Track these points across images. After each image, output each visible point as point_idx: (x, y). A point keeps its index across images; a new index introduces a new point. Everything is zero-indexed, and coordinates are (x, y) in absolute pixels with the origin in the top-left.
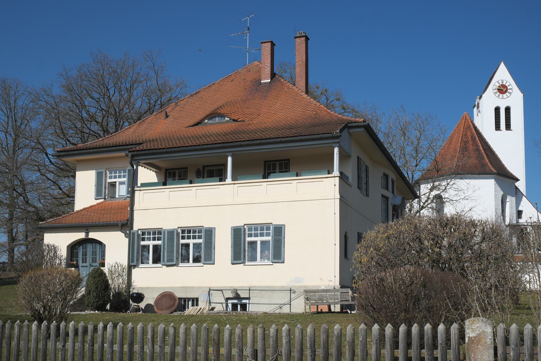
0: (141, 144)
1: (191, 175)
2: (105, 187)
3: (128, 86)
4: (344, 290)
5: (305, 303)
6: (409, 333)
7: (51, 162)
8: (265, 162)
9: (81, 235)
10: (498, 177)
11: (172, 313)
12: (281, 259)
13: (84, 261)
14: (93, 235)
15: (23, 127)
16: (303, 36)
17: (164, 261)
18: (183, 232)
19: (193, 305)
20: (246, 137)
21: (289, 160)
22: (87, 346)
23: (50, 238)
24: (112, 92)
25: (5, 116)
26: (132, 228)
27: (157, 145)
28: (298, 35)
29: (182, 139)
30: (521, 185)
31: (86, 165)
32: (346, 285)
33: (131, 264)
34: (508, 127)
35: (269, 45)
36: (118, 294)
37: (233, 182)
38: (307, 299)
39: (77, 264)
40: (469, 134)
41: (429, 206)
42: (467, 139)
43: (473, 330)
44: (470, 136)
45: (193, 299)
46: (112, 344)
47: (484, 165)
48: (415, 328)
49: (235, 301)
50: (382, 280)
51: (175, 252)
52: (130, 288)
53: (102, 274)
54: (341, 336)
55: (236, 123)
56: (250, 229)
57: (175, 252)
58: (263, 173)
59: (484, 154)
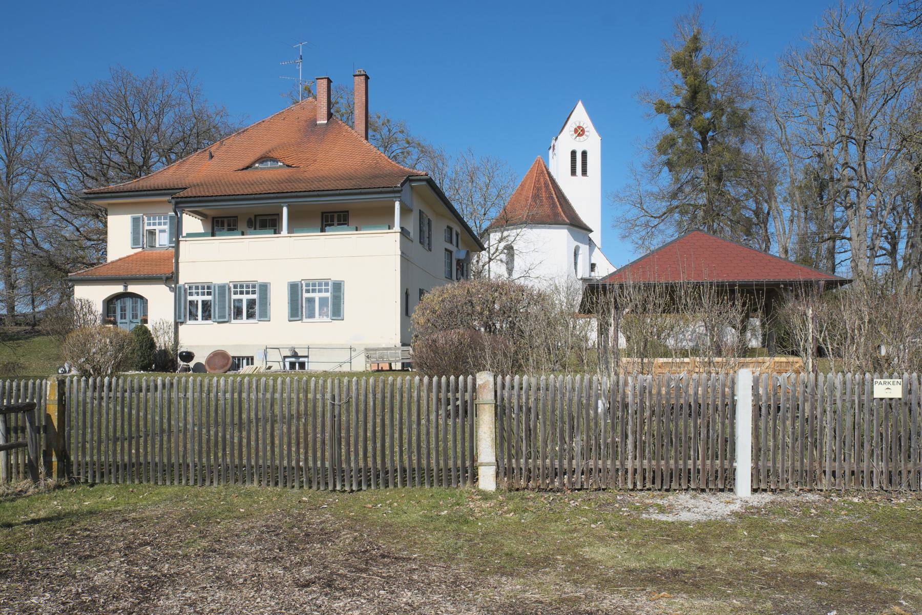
0: (185, 189)
1: (242, 226)
2: (143, 235)
3: (157, 109)
4: (405, 348)
5: (366, 361)
6: (439, 383)
7: (64, 197)
8: (323, 213)
9: (119, 289)
11: (226, 372)
12: (340, 316)
13: (123, 316)
14: (133, 289)
15: (19, 149)
16: (362, 75)
17: (215, 318)
18: (235, 287)
19: (248, 364)
20: (302, 187)
21: (348, 212)
22: (204, 395)
23: (81, 292)
24: (137, 116)
26: (177, 282)
27: (204, 191)
28: (357, 73)
29: (231, 185)
30: (596, 236)
31: (121, 209)
32: (407, 342)
33: (178, 321)
34: (584, 172)
35: (325, 82)
36: (165, 352)
37: (290, 235)
38: (368, 357)
39: (115, 320)
40: (542, 180)
41: (498, 258)
43: (481, 379)
45: (248, 358)
46: (225, 392)
47: (556, 214)
48: (444, 379)
49: (293, 360)
50: (434, 341)
51: (227, 308)
52: (177, 347)
53: (146, 331)
54: (393, 385)
55: (290, 168)
56: (307, 285)
57: (227, 308)
58: (320, 226)
59: (558, 203)
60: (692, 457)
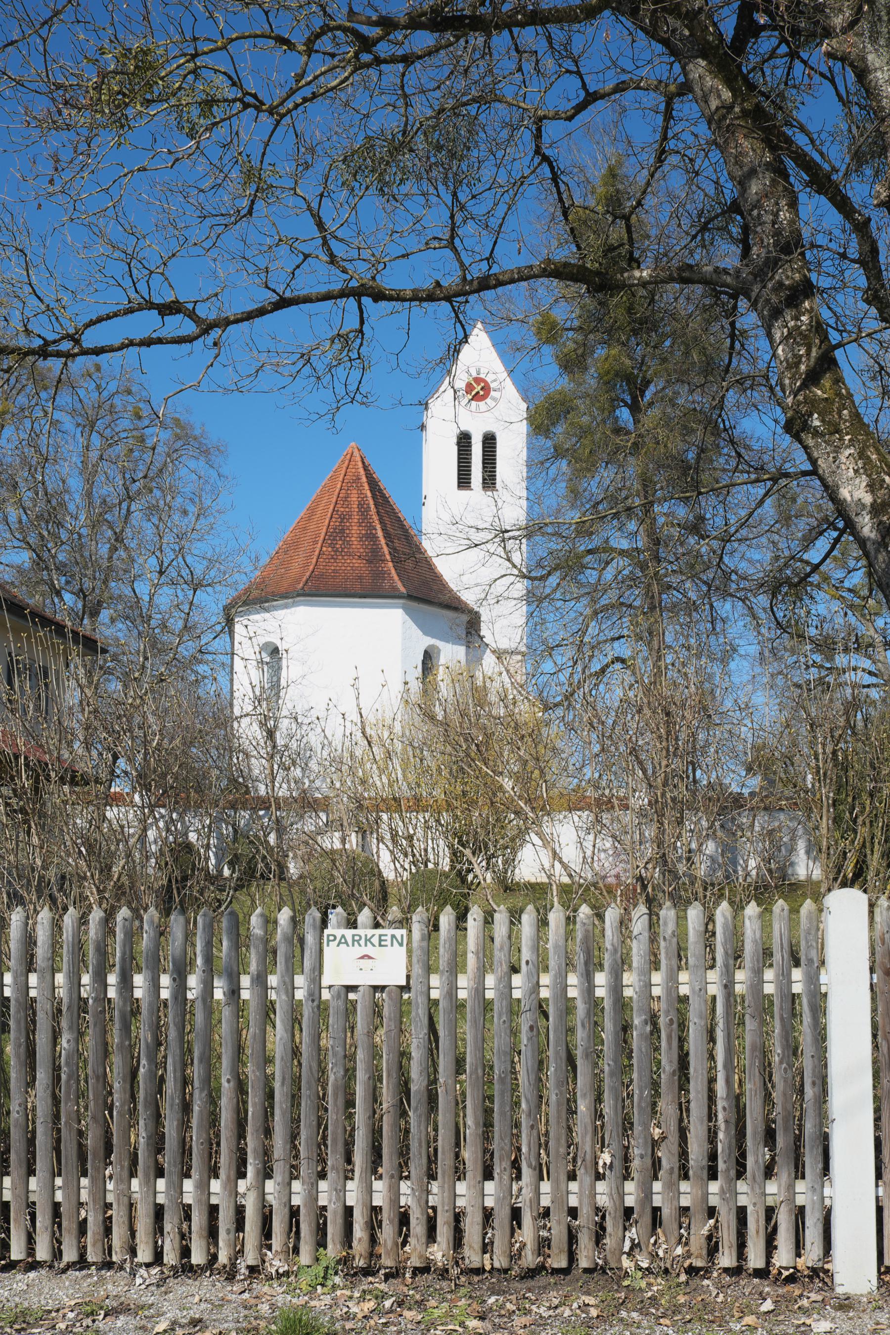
10: (414, 604)
40: (354, 498)
47: (380, 575)
60: (552, 963)
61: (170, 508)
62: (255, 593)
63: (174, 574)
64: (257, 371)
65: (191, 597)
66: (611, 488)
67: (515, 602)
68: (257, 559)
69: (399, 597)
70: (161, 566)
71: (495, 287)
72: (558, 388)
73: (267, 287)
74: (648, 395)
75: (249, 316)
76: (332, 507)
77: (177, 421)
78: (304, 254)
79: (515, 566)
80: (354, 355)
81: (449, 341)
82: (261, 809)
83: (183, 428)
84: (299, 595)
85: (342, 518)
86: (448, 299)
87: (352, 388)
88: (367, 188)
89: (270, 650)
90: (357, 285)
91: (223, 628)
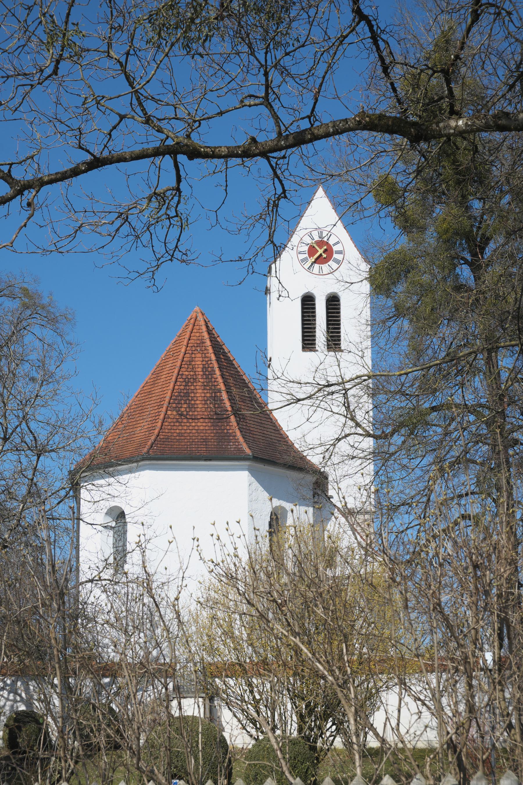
10: (260, 466)
25: (127, 208)
40: (198, 362)
42: (192, 373)
44: (201, 366)
61: (14, 375)
62: (100, 458)
63: (18, 440)
64: (76, 232)
65: (35, 463)
66: (454, 346)
67: (360, 461)
68: (101, 423)
69: (245, 458)
70: (5, 432)
71: (311, 141)
72: (398, 247)
73: (80, 147)
74: (488, 251)
75: (63, 177)
76: (176, 371)
77: (25, 292)
78: (120, 115)
79: (358, 425)
80: (172, 213)
81: (267, 197)
82: (104, 676)
83: (30, 297)
84: (143, 459)
85: (187, 382)
86: (264, 154)
87: (171, 246)
88: (173, 45)
89: (118, 512)
90: (172, 143)
91: (68, 493)
